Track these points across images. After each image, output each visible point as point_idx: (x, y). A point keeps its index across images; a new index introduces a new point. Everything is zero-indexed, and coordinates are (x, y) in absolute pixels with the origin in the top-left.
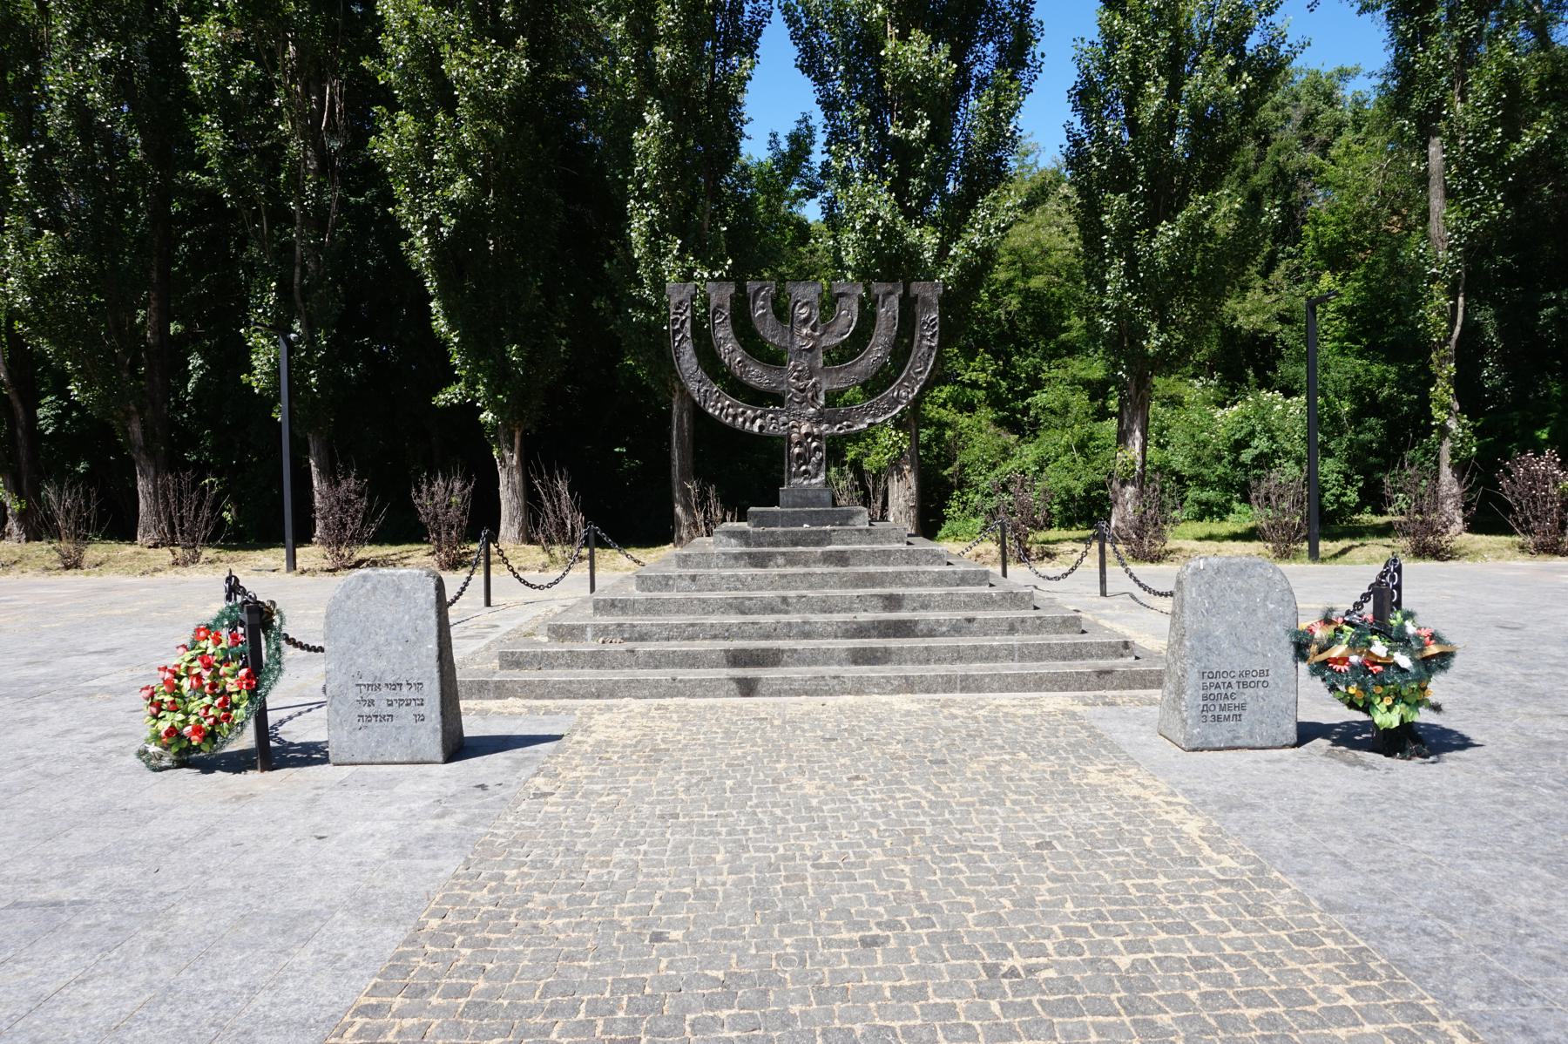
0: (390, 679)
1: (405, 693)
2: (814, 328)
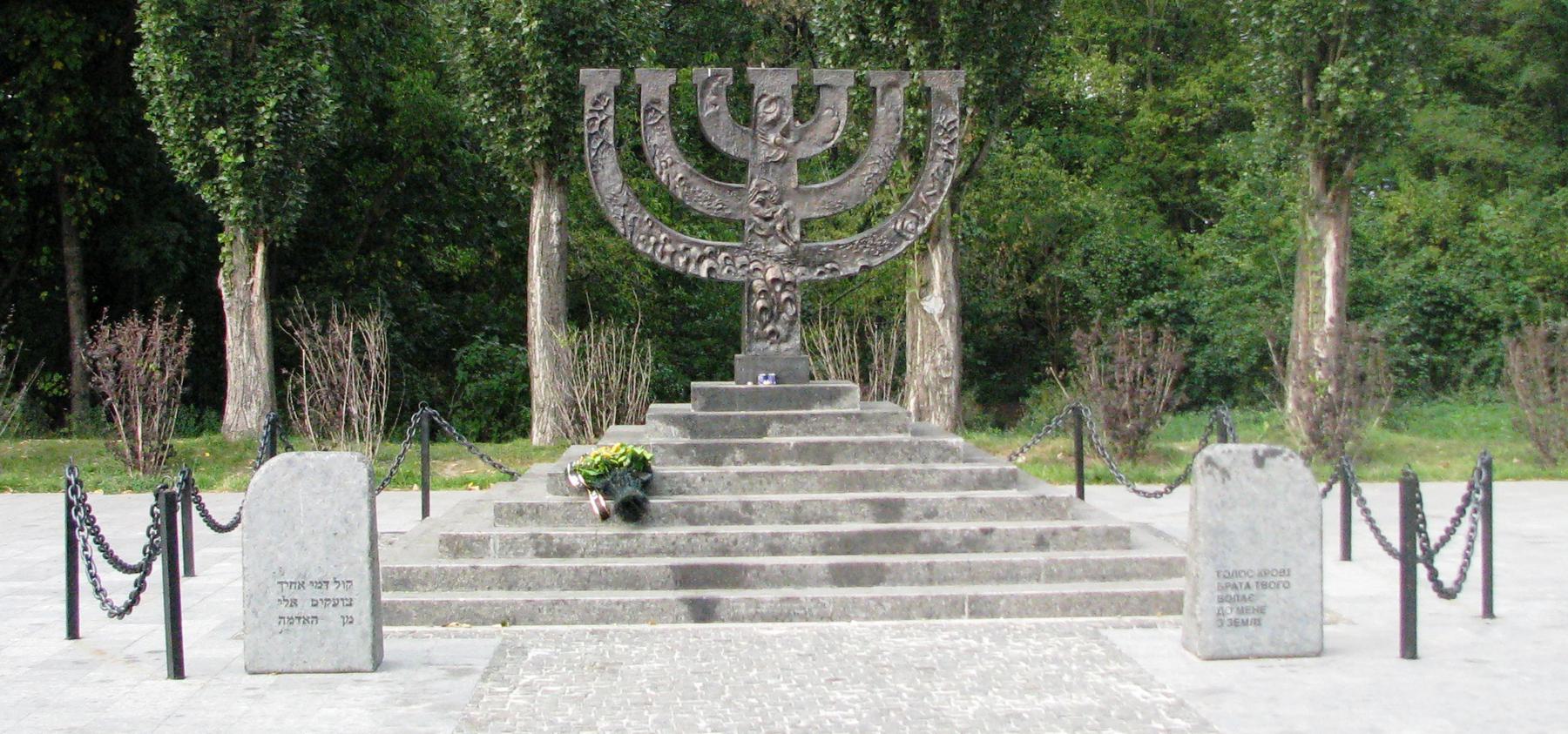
0: (316, 577)
1: (332, 592)
2: (785, 134)
